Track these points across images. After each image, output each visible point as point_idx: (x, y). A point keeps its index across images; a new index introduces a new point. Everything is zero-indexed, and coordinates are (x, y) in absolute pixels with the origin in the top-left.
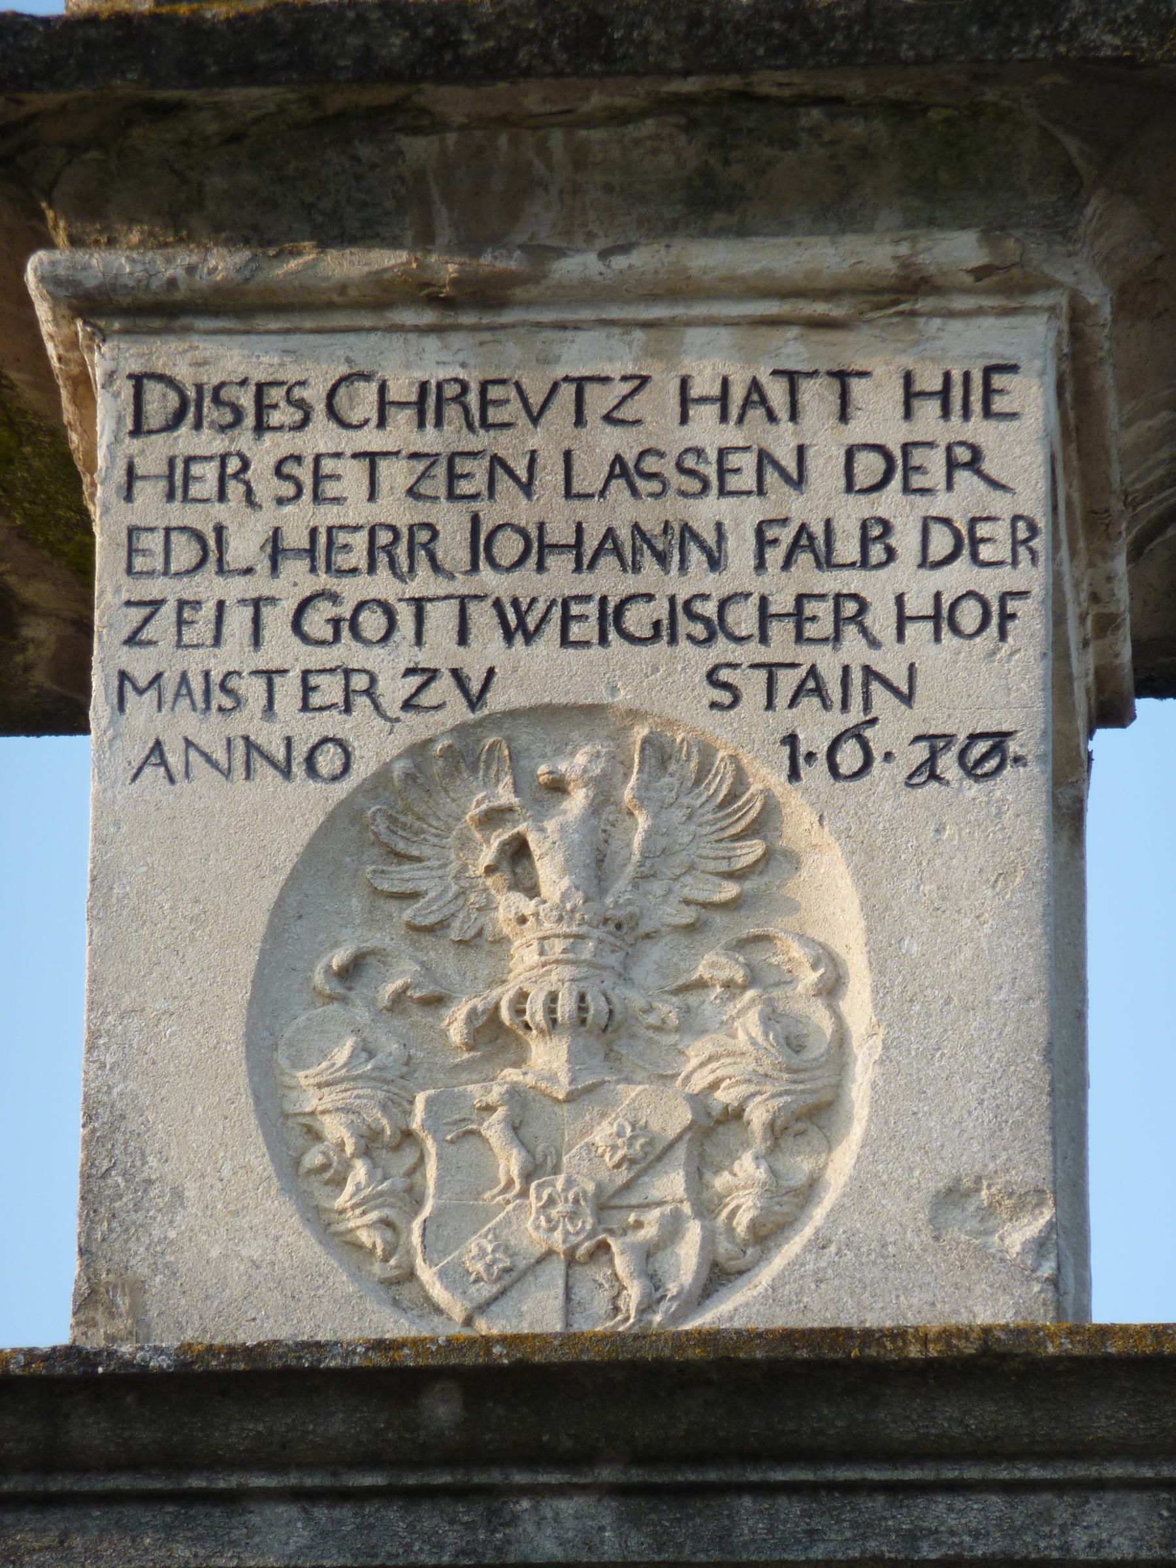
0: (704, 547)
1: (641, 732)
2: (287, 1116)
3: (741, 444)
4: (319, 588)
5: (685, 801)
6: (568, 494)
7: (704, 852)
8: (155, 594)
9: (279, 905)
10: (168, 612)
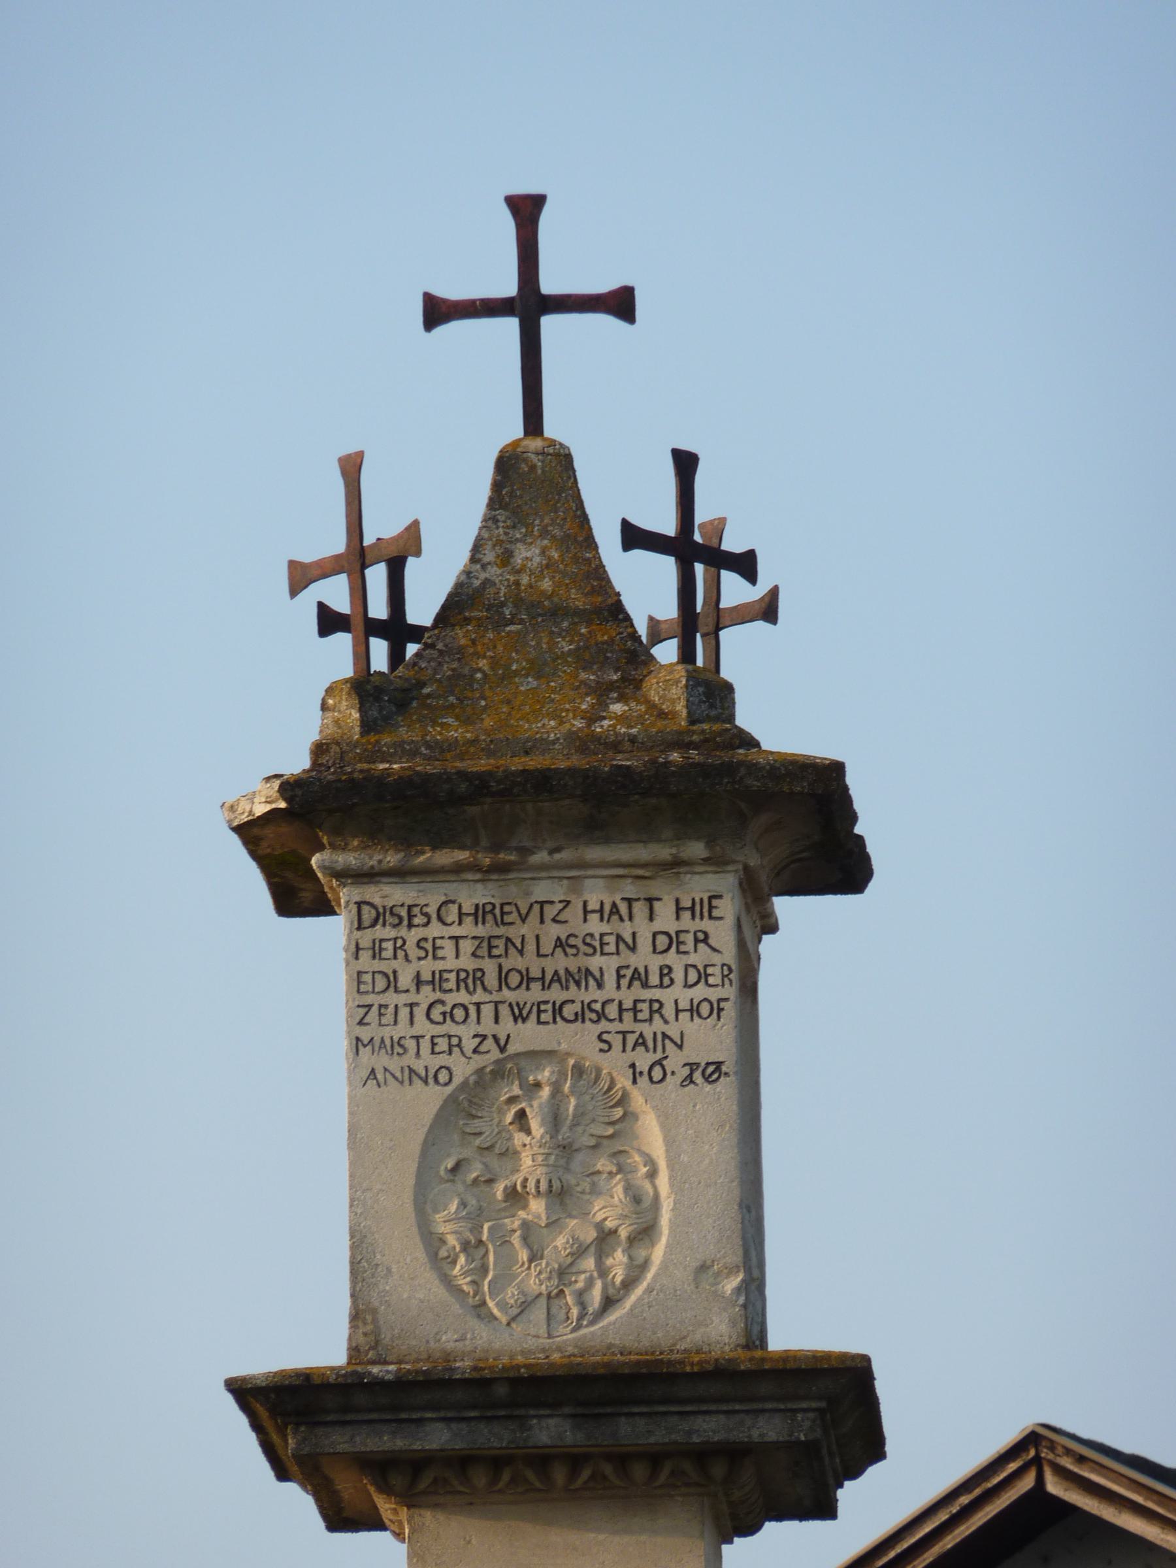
0: (596, 980)
1: (571, 1062)
2: (431, 1233)
3: (609, 932)
4: (436, 998)
5: (591, 1091)
6: (539, 955)
7: (599, 1113)
8: (369, 1002)
9: (425, 1141)
10: (375, 1009)
